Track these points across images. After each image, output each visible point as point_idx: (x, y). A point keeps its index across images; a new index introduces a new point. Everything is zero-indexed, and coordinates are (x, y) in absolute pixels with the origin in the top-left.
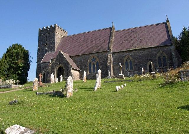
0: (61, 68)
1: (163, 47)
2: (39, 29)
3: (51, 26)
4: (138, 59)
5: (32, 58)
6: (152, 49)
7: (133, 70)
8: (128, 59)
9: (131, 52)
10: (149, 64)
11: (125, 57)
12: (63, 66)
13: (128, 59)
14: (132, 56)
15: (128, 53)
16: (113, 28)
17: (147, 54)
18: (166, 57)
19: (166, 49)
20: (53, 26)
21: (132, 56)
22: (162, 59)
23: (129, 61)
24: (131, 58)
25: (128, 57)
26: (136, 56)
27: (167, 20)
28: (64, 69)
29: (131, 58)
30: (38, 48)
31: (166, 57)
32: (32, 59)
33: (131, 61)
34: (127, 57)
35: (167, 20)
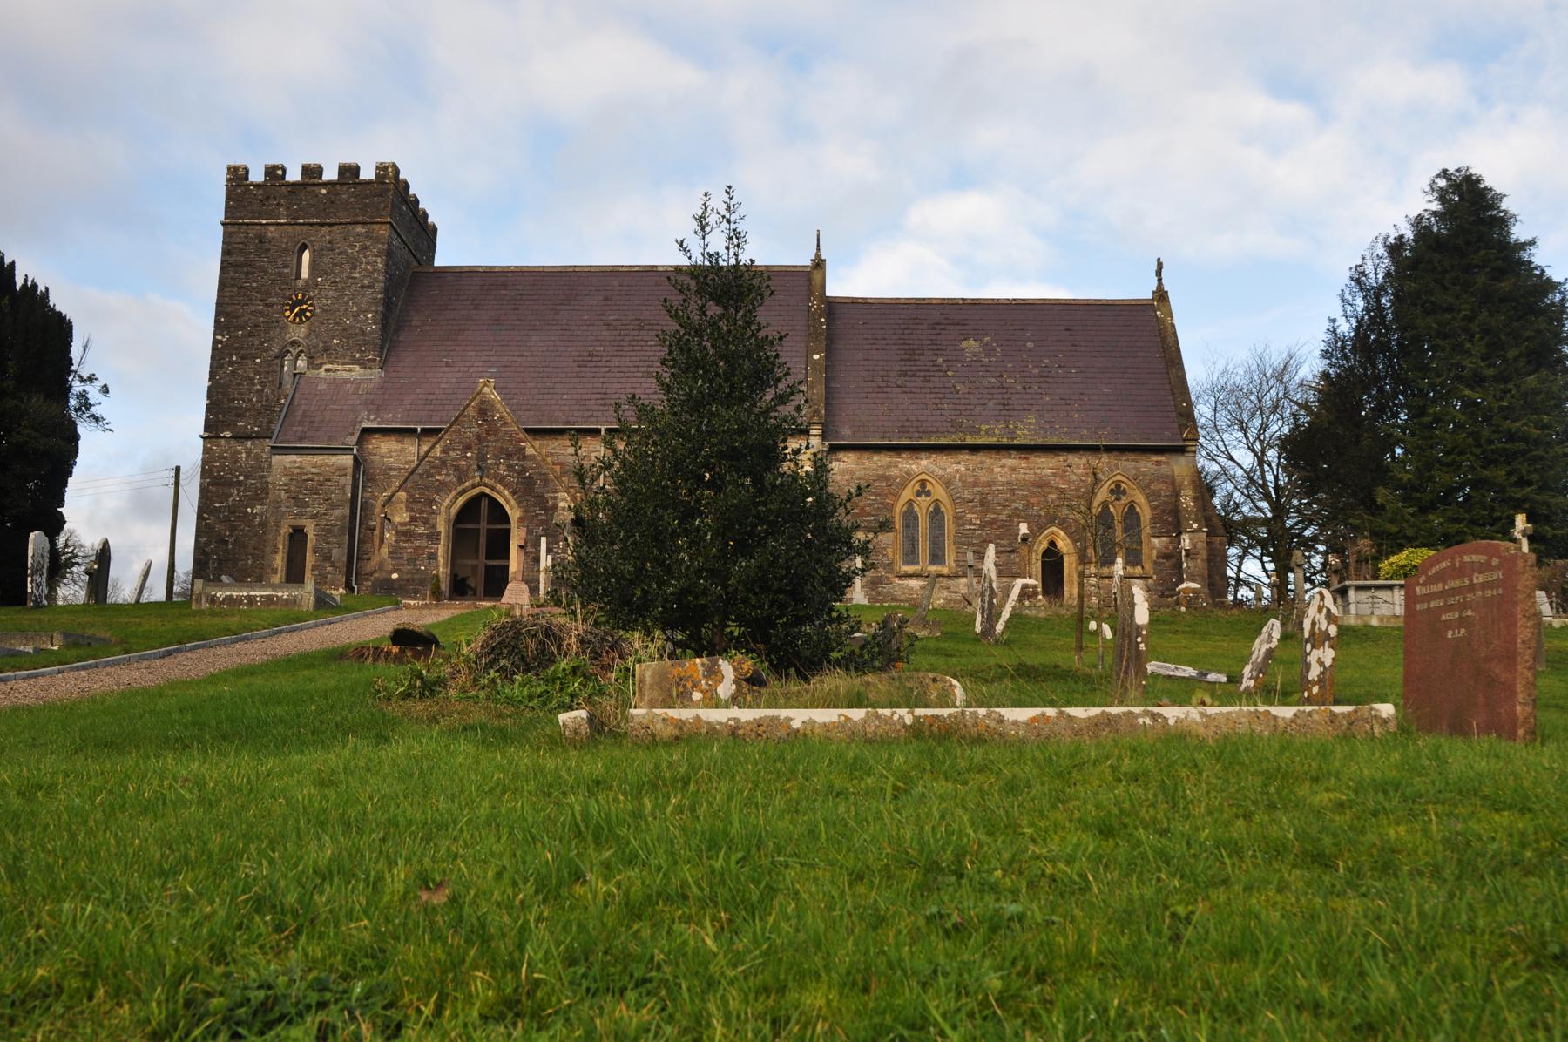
0: (484, 503)
1: (1131, 456)
2: (237, 176)
3: (275, 173)
4: (982, 505)
5: (105, 390)
6: (1072, 458)
7: (945, 570)
8: (919, 494)
9: (1011, 461)
10: (1044, 545)
11: (903, 485)
12: (505, 498)
13: (919, 494)
14: (947, 483)
15: (924, 462)
16: (817, 276)
17: (1042, 484)
18: (1145, 512)
19: (1147, 465)
20: (372, 176)
21: (947, 483)
22: (923, 525)
23: (923, 506)
24: (939, 492)
25: (1118, 486)
26: (975, 484)
27: (818, 256)
28: (514, 513)
29: (939, 492)
30: (217, 322)
31: (1145, 512)
32: (101, 397)
33: (936, 514)
34: (917, 487)
35: (818, 256)
